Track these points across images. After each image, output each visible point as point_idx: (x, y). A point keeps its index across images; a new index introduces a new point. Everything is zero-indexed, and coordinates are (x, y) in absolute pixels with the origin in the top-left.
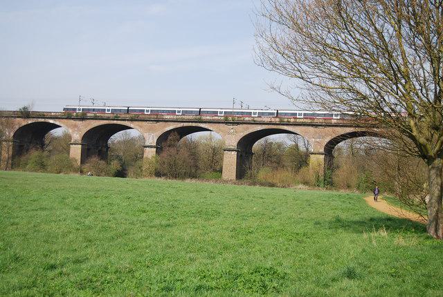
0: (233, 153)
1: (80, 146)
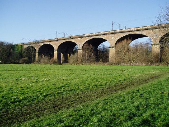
0: (114, 48)
1: (57, 52)
